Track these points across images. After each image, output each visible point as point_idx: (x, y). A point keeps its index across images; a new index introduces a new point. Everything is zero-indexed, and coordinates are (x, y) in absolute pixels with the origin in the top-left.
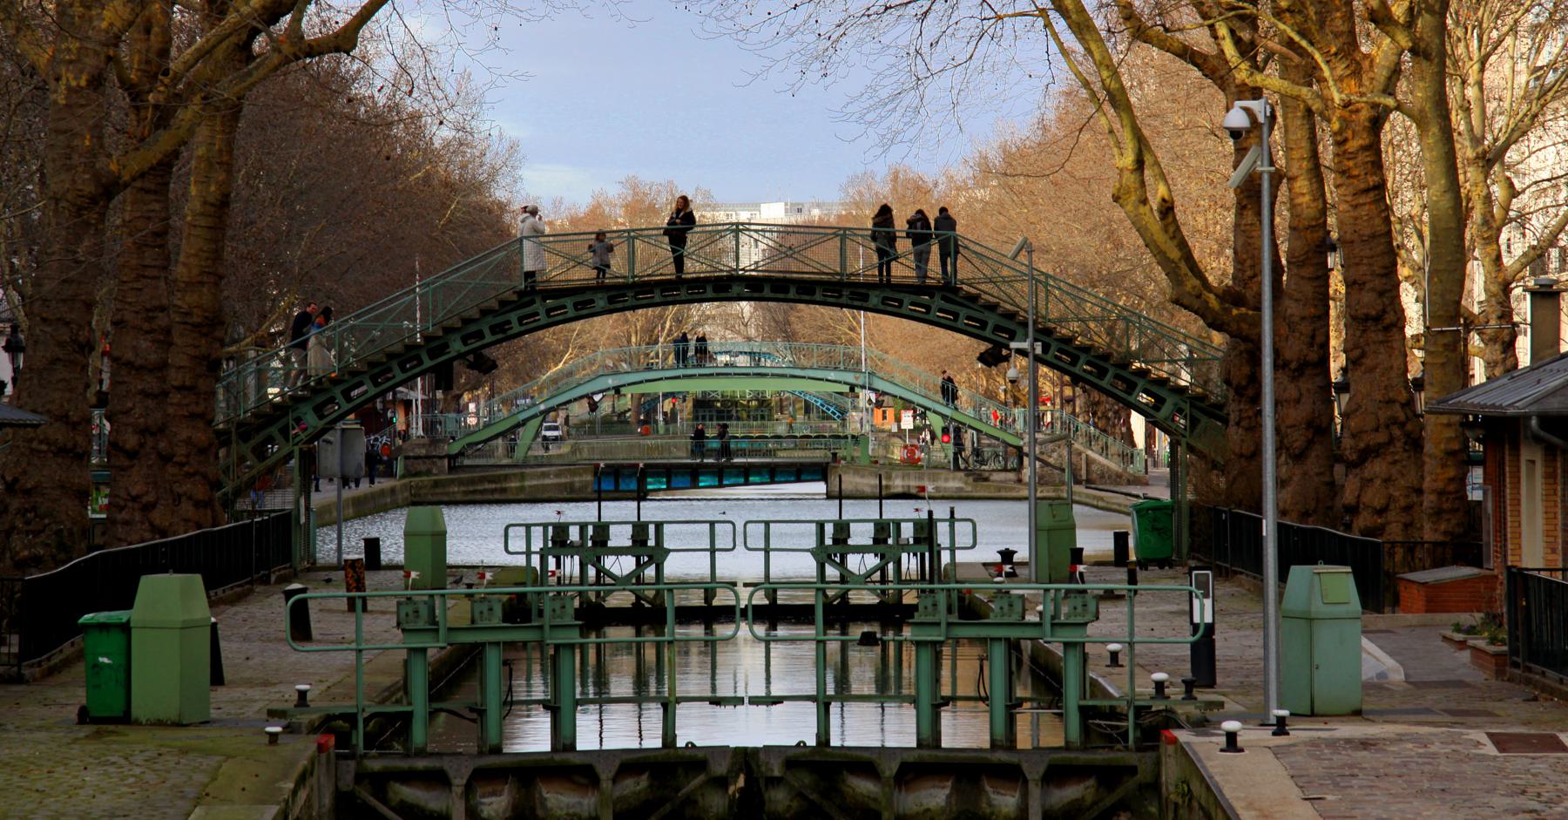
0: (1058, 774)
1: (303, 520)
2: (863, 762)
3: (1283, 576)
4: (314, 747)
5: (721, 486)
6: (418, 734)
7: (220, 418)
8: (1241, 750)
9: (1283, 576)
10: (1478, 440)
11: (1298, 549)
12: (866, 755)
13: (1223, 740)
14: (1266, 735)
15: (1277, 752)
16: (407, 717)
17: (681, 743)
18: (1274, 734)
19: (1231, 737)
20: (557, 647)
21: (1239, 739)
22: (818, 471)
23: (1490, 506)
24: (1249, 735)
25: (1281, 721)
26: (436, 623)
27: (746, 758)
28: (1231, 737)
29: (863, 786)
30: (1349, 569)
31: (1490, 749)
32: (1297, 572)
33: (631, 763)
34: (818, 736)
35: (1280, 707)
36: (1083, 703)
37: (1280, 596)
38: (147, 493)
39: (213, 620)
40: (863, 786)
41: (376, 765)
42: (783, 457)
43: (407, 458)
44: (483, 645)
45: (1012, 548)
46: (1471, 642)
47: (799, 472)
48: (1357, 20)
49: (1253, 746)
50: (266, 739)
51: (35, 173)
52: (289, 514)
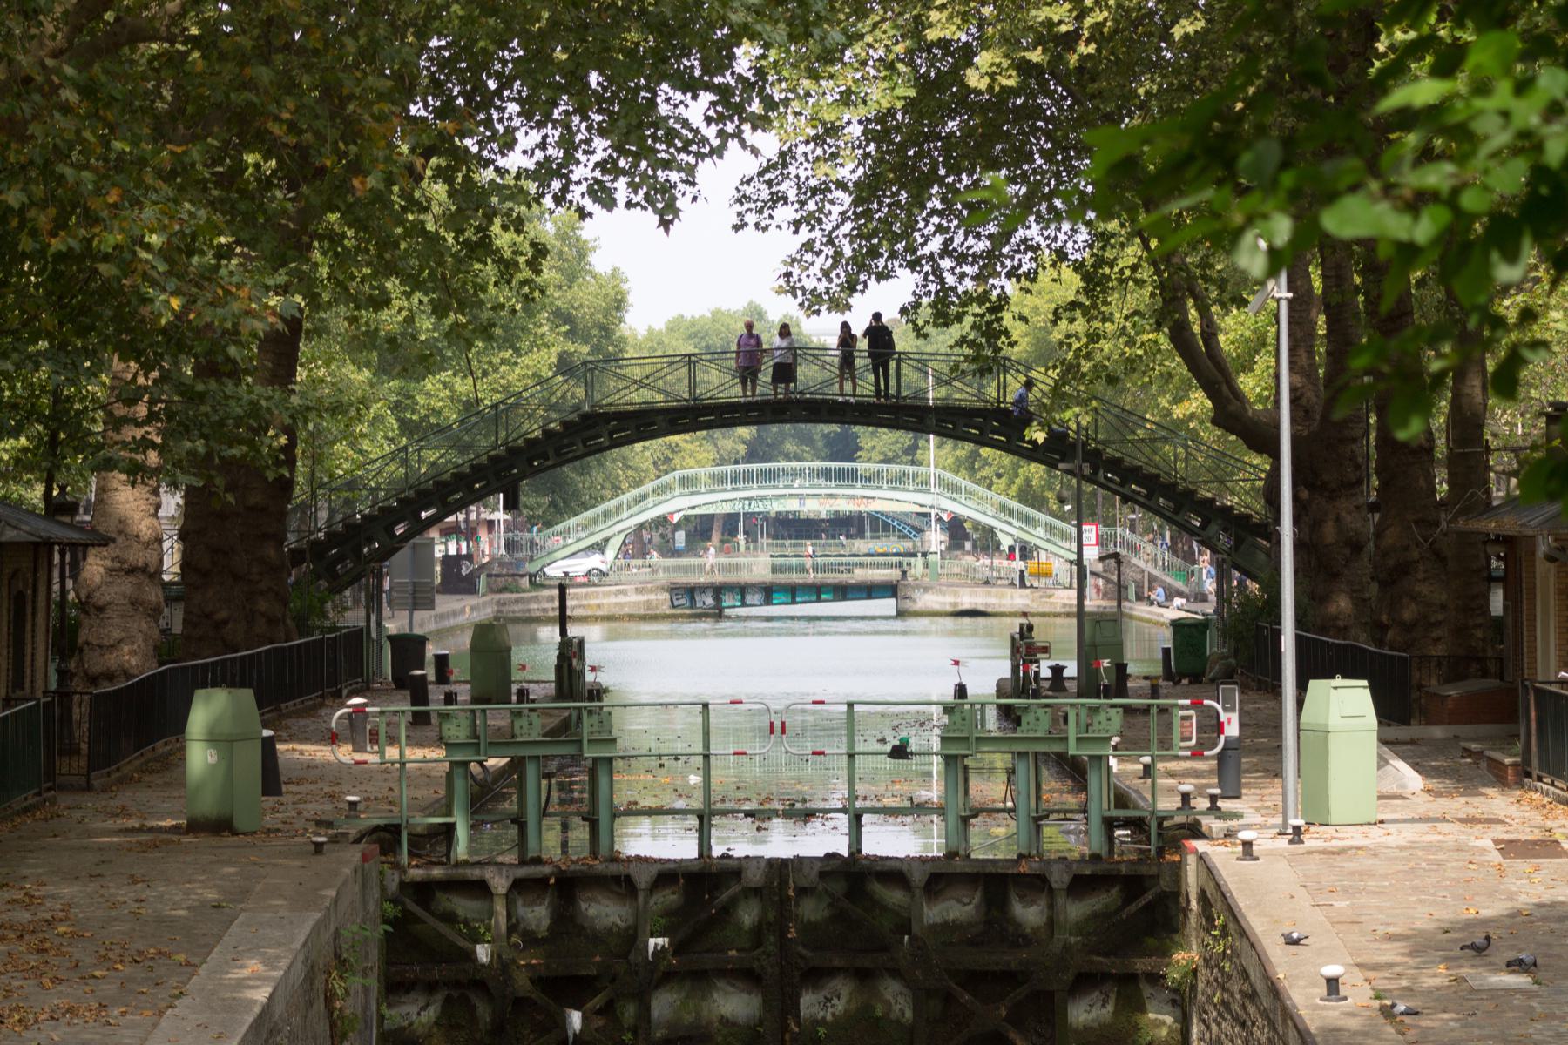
0: (1081, 884)
1: (374, 635)
2: (892, 872)
3: (1302, 687)
4: (358, 856)
5: (794, 602)
6: (461, 849)
7: (291, 537)
8: (1257, 859)
9: (1302, 687)
10: (1499, 558)
11: (1315, 665)
12: (898, 864)
13: (1240, 848)
14: (1283, 843)
15: (1291, 859)
16: (449, 829)
17: (717, 851)
18: (1291, 842)
19: (1247, 845)
20: (595, 760)
21: (1255, 848)
22: (889, 590)
23: (1510, 620)
24: (1265, 843)
25: (1297, 829)
26: (477, 737)
27: (780, 868)
28: (1247, 845)
29: (894, 897)
30: (1365, 683)
31: (1496, 857)
32: (1315, 685)
33: (668, 874)
34: (850, 847)
35: (1296, 817)
36: (1107, 814)
37: (1300, 703)
38: (798, 1024)
39: (267, 733)
40: (894, 897)
41: (416, 874)
42: (860, 575)
43: (489, 576)
44: (523, 758)
45: (1062, 663)
46: (1487, 753)
47: (870, 591)
48: (929, 349)
49: (1270, 853)
50: (312, 847)
51: (162, 401)
52: (361, 630)
